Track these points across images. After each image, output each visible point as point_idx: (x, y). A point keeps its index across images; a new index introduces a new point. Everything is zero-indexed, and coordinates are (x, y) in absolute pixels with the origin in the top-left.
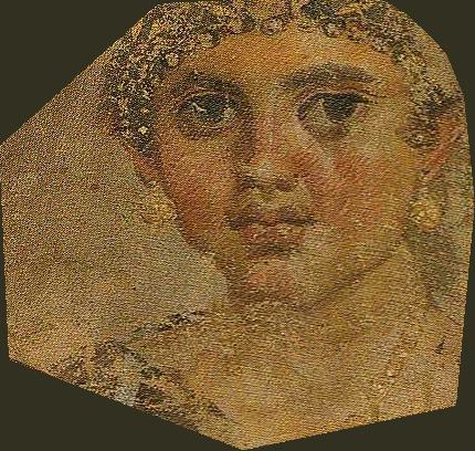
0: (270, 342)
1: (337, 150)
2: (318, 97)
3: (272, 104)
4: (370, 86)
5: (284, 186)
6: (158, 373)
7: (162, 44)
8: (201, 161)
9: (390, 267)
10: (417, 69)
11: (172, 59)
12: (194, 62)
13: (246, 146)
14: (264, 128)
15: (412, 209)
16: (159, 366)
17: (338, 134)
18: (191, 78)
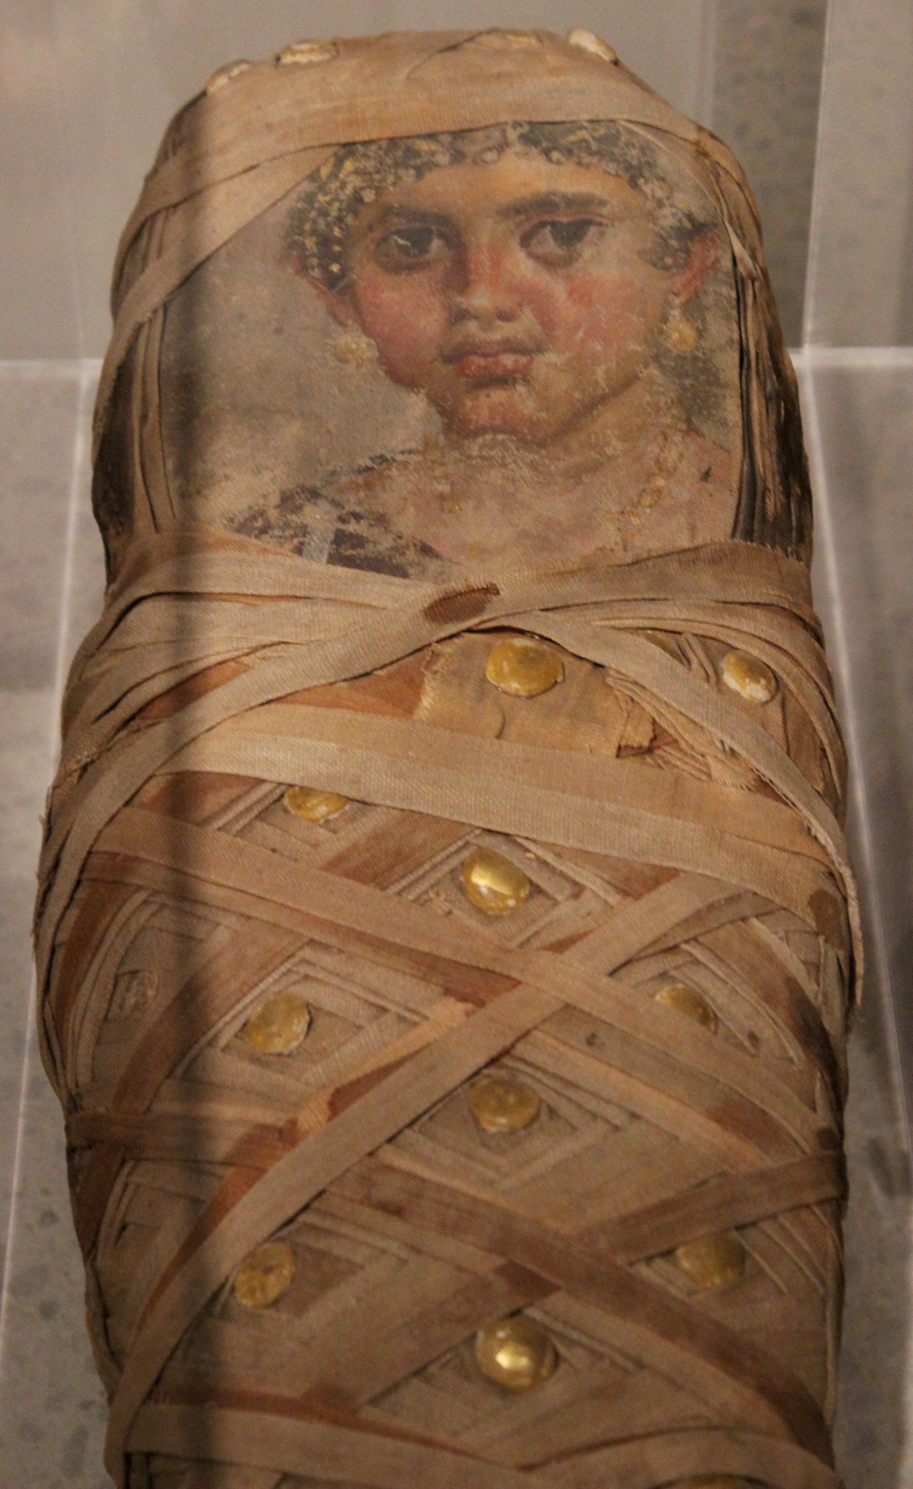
0: (495, 476)
1: (569, 278)
2: (543, 225)
3: (485, 234)
4: (605, 211)
5: (505, 316)
6: (357, 517)
7: (355, 181)
8: (412, 305)
9: (640, 395)
10: (660, 194)
11: (369, 196)
12: (394, 196)
13: (460, 276)
14: (481, 258)
15: (661, 332)
16: (358, 509)
17: (568, 261)
18: (387, 211)
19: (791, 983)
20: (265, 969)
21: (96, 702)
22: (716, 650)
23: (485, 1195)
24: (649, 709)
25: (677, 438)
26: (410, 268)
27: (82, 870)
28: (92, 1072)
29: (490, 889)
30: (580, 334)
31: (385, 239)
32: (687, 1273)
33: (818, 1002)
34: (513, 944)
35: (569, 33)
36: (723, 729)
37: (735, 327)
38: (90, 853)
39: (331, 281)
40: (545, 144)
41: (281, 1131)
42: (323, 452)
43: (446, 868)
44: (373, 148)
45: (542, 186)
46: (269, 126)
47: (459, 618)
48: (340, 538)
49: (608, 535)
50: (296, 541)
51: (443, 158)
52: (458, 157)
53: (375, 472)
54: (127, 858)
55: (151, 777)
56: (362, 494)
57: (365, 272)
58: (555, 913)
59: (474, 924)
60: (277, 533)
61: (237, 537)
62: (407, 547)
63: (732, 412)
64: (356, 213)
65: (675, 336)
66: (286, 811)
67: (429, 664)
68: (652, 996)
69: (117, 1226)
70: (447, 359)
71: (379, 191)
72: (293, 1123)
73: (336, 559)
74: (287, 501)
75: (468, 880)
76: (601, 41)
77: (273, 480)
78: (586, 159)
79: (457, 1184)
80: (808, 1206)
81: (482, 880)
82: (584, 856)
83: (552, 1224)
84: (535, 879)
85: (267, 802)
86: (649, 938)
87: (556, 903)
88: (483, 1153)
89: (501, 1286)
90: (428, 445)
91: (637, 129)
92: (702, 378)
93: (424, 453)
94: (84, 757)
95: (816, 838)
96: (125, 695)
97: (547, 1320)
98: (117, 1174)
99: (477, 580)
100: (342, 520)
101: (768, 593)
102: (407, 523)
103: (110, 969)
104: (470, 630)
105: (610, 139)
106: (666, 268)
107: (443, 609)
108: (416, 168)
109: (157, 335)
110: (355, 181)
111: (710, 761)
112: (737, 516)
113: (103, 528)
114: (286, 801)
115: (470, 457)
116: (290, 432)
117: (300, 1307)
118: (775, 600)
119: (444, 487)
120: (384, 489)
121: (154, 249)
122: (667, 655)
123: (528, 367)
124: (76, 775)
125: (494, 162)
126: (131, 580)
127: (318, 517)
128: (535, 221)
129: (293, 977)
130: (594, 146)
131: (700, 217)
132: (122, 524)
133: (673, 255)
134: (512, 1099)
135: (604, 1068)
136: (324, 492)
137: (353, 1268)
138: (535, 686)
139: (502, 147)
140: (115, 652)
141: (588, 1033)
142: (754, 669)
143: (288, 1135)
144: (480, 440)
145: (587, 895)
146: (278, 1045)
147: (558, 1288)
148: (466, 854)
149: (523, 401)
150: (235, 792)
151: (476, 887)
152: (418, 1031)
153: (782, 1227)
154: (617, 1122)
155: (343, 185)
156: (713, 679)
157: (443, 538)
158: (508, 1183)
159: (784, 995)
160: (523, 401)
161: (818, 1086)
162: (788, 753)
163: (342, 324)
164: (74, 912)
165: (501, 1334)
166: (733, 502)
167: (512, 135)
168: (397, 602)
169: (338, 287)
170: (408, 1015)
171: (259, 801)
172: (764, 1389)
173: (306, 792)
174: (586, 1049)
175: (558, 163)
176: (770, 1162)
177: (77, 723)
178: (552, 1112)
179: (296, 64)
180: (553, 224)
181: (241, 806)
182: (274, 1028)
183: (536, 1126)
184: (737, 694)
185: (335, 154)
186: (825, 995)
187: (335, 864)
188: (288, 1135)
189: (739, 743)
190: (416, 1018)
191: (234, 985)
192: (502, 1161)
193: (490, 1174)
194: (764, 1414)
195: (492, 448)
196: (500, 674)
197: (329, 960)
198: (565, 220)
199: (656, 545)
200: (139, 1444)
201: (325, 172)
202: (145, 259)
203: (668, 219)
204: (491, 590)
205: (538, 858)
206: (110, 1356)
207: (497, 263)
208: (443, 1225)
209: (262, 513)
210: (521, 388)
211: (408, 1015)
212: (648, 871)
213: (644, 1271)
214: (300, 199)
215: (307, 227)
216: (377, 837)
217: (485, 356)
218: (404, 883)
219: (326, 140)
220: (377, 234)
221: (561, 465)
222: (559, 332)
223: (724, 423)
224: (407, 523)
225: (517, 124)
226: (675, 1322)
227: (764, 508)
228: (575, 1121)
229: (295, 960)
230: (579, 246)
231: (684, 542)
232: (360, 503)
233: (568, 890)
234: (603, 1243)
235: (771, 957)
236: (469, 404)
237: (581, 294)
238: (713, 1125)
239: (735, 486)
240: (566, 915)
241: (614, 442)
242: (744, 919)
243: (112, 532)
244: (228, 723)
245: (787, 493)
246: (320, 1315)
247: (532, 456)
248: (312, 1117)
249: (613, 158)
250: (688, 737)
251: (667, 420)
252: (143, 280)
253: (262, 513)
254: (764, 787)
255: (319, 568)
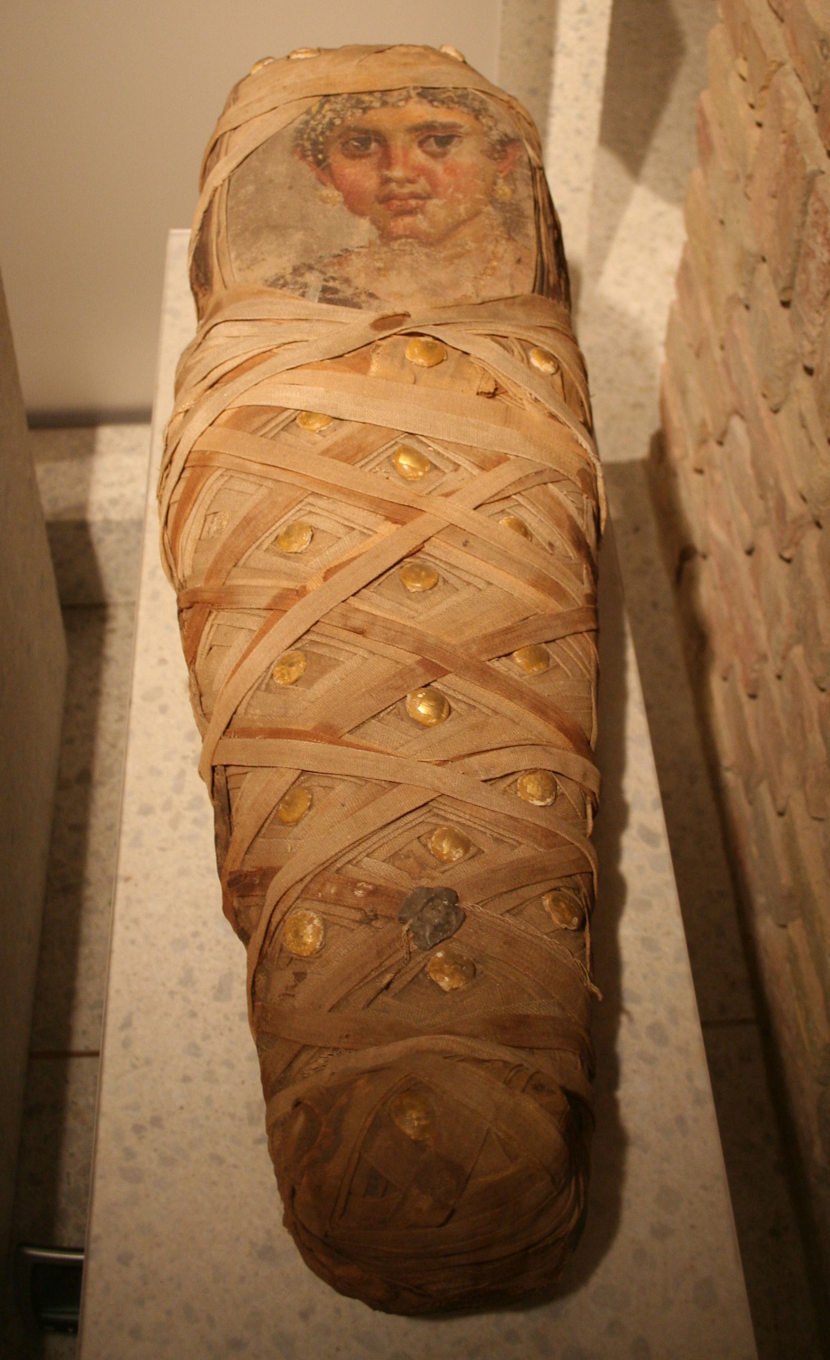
0: (408, 259)
2: (430, 137)
3: (399, 142)
4: (462, 130)
5: (411, 182)
6: (334, 279)
8: (361, 174)
10: (491, 124)
11: (338, 122)
13: (386, 160)
15: (493, 190)
16: (334, 275)
17: (444, 154)
19: (570, 517)
20: (287, 508)
21: (193, 377)
22: (527, 346)
23: (410, 623)
24: (493, 374)
25: (503, 242)
26: (361, 157)
27: (186, 461)
28: (193, 567)
29: (409, 466)
30: (451, 190)
31: (347, 142)
32: (517, 666)
33: (584, 529)
34: (424, 493)
35: (441, 47)
36: (531, 387)
37: (531, 189)
38: (190, 452)
39: (318, 163)
40: (430, 98)
41: (297, 591)
42: (315, 247)
43: (385, 455)
44: (340, 99)
45: (429, 118)
46: (284, 88)
47: (390, 328)
48: (325, 290)
49: (468, 289)
50: (301, 291)
51: (377, 104)
52: (384, 104)
53: (342, 257)
54: (212, 453)
55: (224, 411)
56: (336, 268)
57: (337, 159)
58: (444, 479)
59: (400, 484)
60: (291, 286)
61: (269, 289)
62: (361, 293)
63: (531, 230)
64: (331, 130)
65: (501, 192)
66: (298, 426)
67: (374, 351)
68: (498, 521)
69: (207, 647)
70: (381, 202)
71: (343, 119)
72: (304, 587)
73: (321, 300)
74: (296, 271)
75: (397, 461)
76: (457, 51)
77: (289, 260)
78: (452, 105)
79: (393, 618)
80: (581, 633)
81: (405, 462)
82: (459, 447)
83: (447, 639)
84: (433, 461)
85: (287, 422)
86: (494, 491)
87: (444, 473)
88: (409, 602)
89: (420, 670)
90: (371, 244)
91: (477, 93)
92: (516, 213)
93: (369, 248)
94: (186, 406)
95: (581, 445)
96: (209, 373)
97: (444, 689)
98: (207, 620)
99: (399, 310)
100: (325, 280)
101: (551, 322)
102: (361, 281)
103: (202, 512)
104: (395, 334)
105: (464, 96)
106: (495, 159)
107: (381, 323)
108: (362, 108)
109: (225, 191)
110: (330, 115)
111: (525, 402)
112: (535, 285)
113: (196, 295)
114: (297, 421)
115: (394, 250)
116: (298, 237)
117: (310, 683)
118: (555, 326)
119: (380, 264)
120: (348, 265)
121: (223, 151)
122: (501, 348)
123: (424, 205)
124: (182, 415)
125: (403, 106)
126: (211, 316)
127: (313, 279)
128: (426, 134)
129: (303, 513)
130: (456, 99)
131: (512, 136)
132: (206, 290)
133: (499, 152)
134: (423, 574)
135: (472, 558)
136: (316, 267)
137: (337, 663)
138: (432, 362)
139: (408, 99)
140: (203, 351)
141: (464, 540)
142: (547, 357)
143: (301, 593)
144: (399, 242)
145: (461, 469)
146: (295, 548)
147: (449, 672)
148: (396, 448)
149: (421, 222)
150: (271, 415)
151: (401, 465)
152: (371, 539)
153: (569, 645)
154: (480, 586)
155: (324, 117)
156: (526, 361)
157: (381, 287)
158: (422, 618)
159: (567, 524)
160: (421, 222)
161: (585, 572)
162: (565, 400)
163: (324, 184)
164: (182, 484)
165: (420, 696)
166: (532, 275)
167: (413, 93)
168: (355, 323)
169: (321, 165)
170: (365, 531)
171: (283, 421)
172: (561, 728)
173: (309, 414)
174: (463, 548)
175: (437, 107)
176: (561, 609)
177: (183, 390)
178: (445, 581)
179: (299, 60)
180: (435, 137)
181: (273, 424)
182: (293, 539)
183: (436, 589)
184: (538, 369)
185: (320, 101)
186: (587, 525)
187: (325, 452)
188: (301, 593)
189: (540, 395)
190: (370, 533)
191: (271, 517)
192: (419, 607)
193: (412, 613)
194: (560, 739)
195: (405, 245)
196: (413, 354)
197: (321, 503)
198: (440, 134)
199: (494, 294)
200: (219, 761)
201: (314, 110)
202: (218, 156)
203: (495, 135)
204: (406, 315)
205: (435, 451)
206: (203, 714)
207: (406, 155)
208: (387, 639)
209: (283, 277)
210: (420, 216)
211: (365, 531)
212: (494, 458)
213: (496, 664)
214: (301, 123)
215: (305, 136)
216: (349, 438)
217: (400, 200)
218: (363, 463)
219: (315, 94)
220: (342, 140)
221: (442, 255)
222: (440, 189)
223: (527, 236)
224: (361, 281)
225: (415, 88)
226: (513, 691)
227: (548, 280)
228: (459, 587)
229: (304, 503)
230: (449, 147)
231: (508, 293)
232: (335, 272)
233: (451, 467)
234: (474, 648)
235: (560, 504)
236: (392, 224)
237: (451, 170)
238: (531, 588)
239: (534, 267)
240: (451, 479)
241: (470, 243)
242: (545, 484)
243: (200, 295)
244: (266, 381)
245: (559, 275)
246: (321, 687)
247: (427, 250)
248: (314, 584)
249: (466, 105)
250: (512, 390)
251: (497, 233)
252: (218, 167)
253: (283, 277)
254: (553, 416)
255: (313, 305)
